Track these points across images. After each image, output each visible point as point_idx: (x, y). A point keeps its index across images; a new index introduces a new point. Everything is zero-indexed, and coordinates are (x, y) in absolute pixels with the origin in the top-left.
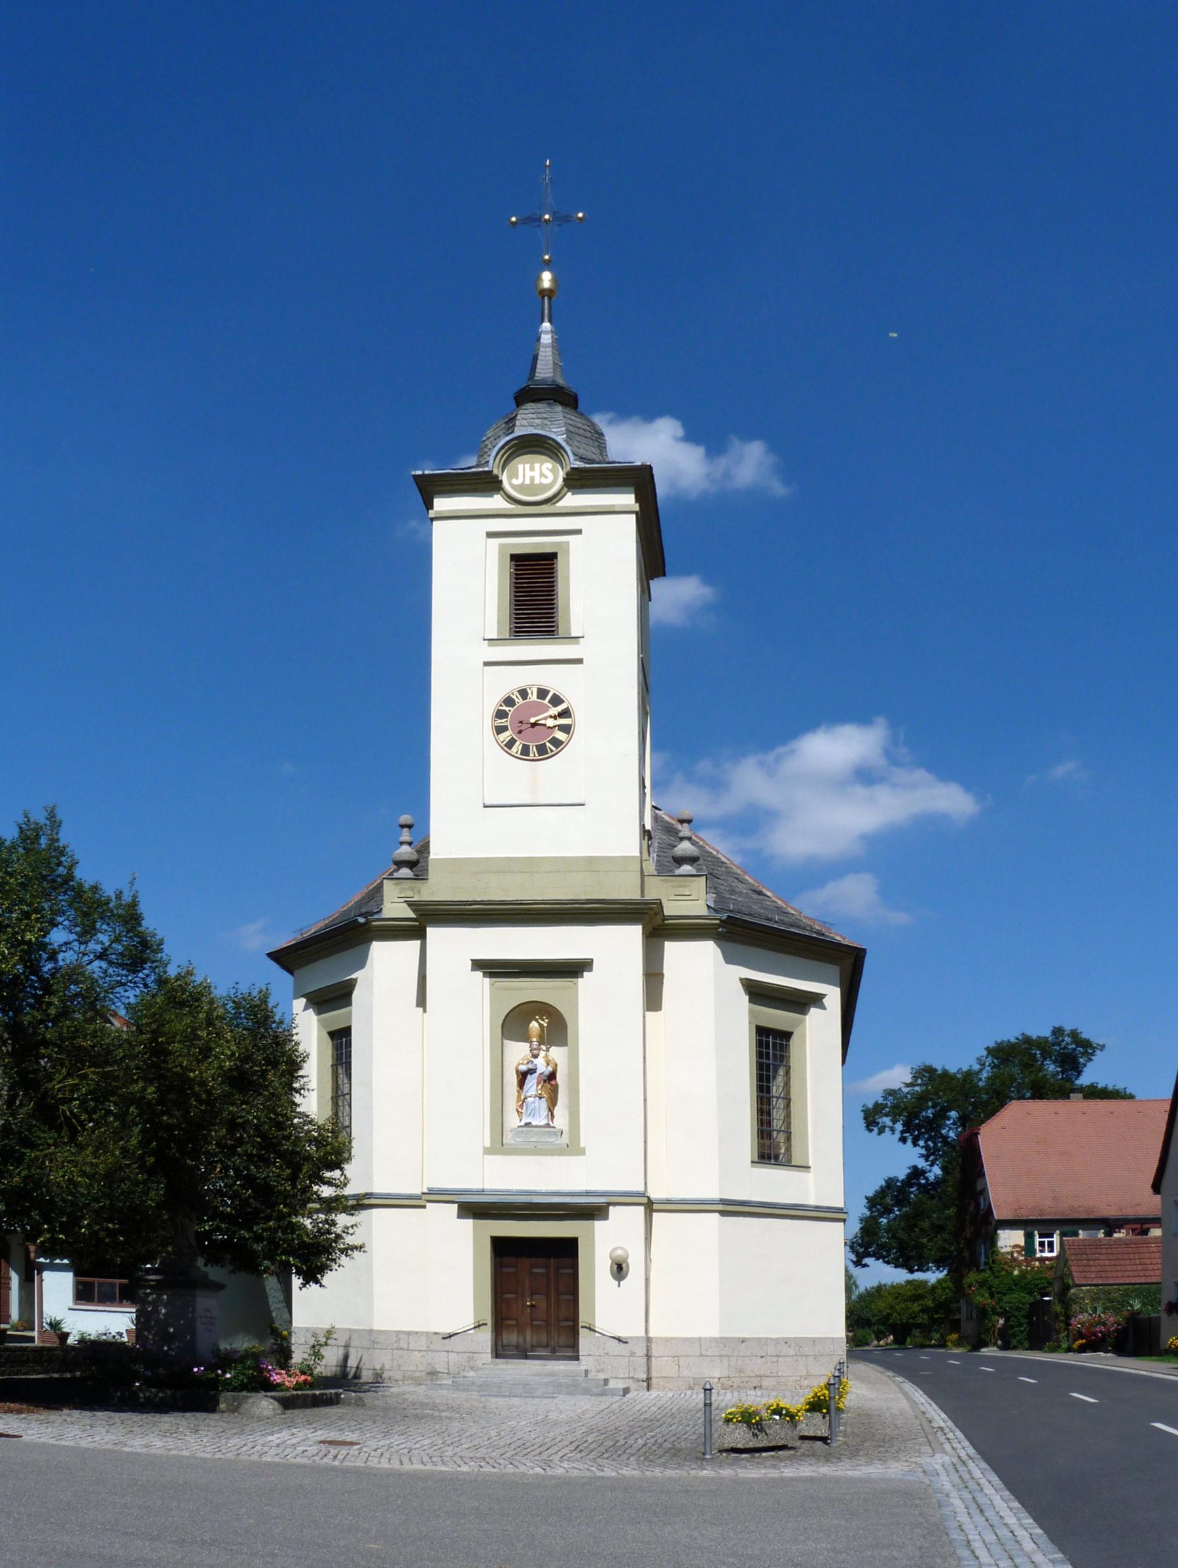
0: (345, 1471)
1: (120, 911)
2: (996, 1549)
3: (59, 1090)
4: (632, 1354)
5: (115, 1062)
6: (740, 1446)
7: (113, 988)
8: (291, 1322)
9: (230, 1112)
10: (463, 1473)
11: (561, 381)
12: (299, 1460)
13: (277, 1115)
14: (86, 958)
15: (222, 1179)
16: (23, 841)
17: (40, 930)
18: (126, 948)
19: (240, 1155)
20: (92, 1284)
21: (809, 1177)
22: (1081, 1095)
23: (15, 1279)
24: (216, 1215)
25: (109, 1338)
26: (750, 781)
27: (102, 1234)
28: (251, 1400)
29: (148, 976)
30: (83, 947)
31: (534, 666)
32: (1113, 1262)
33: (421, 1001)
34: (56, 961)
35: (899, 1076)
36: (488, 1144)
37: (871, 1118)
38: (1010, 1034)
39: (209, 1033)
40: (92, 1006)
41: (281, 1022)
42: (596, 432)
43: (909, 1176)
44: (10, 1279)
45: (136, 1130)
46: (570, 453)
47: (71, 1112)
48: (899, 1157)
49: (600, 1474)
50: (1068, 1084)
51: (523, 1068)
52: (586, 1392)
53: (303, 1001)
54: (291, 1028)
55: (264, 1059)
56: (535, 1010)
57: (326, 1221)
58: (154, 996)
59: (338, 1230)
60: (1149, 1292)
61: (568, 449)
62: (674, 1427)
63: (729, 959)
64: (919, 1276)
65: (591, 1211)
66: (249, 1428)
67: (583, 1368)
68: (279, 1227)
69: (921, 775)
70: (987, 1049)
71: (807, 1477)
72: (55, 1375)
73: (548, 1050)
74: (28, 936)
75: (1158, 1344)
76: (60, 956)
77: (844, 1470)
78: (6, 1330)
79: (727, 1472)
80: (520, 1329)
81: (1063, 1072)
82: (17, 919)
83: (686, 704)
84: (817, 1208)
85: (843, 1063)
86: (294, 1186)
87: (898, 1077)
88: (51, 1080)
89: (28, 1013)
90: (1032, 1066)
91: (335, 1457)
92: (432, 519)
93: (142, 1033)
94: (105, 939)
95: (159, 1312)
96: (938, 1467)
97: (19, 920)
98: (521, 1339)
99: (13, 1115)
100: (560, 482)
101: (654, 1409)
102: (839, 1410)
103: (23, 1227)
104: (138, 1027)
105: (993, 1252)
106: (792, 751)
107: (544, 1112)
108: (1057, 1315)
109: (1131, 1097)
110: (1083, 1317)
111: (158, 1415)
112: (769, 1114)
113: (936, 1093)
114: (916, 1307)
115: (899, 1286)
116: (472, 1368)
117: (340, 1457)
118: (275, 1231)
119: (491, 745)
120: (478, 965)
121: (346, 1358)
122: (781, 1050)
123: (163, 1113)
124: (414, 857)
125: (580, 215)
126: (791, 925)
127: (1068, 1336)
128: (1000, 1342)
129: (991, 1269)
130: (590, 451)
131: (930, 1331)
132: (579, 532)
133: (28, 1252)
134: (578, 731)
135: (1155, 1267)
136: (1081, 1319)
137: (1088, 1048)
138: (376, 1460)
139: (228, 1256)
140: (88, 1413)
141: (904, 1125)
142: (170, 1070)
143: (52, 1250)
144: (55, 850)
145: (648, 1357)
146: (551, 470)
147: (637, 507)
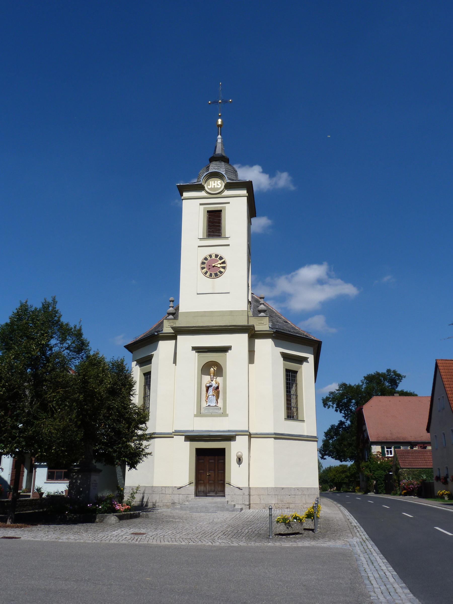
0: (140, 546)
1: (75, 332)
2: (379, 580)
3: (49, 397)
4: (244, 494)
5: (70, 387)
6: (282, 533)
10: (183, 545)
11: (224, 154)
12: (124, 542)
13: (124, 404)
14: (62, 349)
15: (104, 429)
16: (44, 308)
17: (47, 340)
19: (111, 420)
20: (54, 472)
21: (304, 424)
23: (26, 471)
24: (101, 443)
26: (283, 284)
27: (60, 452)
28: (108, 517)
29: (83, 355)
30: (61, 345)
31: (214, 247)
32: (414, 459)
33: (175, 362)
34: (52, 350)
35: (334, 387)
37: (325, 402)
38: (372, 372)
39: (103, 375)
40: (63, 366)
41: (128, 370)
43: (339, 424)
44: (24, 472)
45: (75, 412)
47: (53, 406)
48: (336, 417)
49: (232, 545)
50: (393, 390)
51: (208, 385)
52: (227, 510)
53: (135, 362)
54: (131, 372)
55: (121, 384)
58: (85, 362)
59: (143, 447)
60: (429, 472)
61: (226, 176)
62: (258, 525)
63: (277, 345)
64: (344, 463)
65: (229, 438)
67: (226, 500)
69: (339, 281)
70: (364, 377)
72: (37, 511)
73: (216, 378)
74: (43, 342)
76: (53, 349)
78: (20, 493)
79: (278, 544)
80: (205, 484)
81: (391, 386)
84: (308, 436)
88: (46, 394)
90: (380, 383)
91: (137, 540)
92: (183, 200)
93: (80, 376)
94: (69, 342)
96: (355, 543)
97: (40, 336)
98: (205, 489)
101: (251, 517)
102: (318, 518)
105: (370, 454)
106: (297, 274)
107: (215, 401)
108: (395, 480)
109: (416, 395)
110: (405, 481)
111: (73, 525)
112: (290, 401)
113: (347, 393)
114: (343, 476)
116: (187, 501)
117: (139, 540)
119: (200, 273)
120: (194, 348)
121: (143, 498)
122: (294, 378)
127: (400, 489)
129: (370, 461)
130: (233, 177)
132: (229, 203)
133: (32, 461)
134: (228, 268)
138: (151, 541)
139: (104, 459)
140: (47, 526)
141: (337, 405)
142: (88, 389)
145: (249, 495)
147: (247, 195)
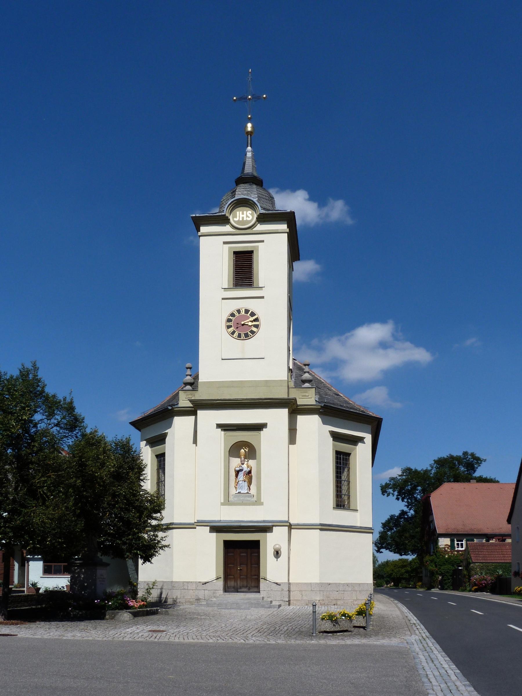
1: (65, 406)
2: (439, 678)
3: (38, 483)
4: (282, 590)
5: (63, 470)
6: (328, 630)
11: (255, 174)
12: (140, 639)
14: (50, 426)
15: (109, 518)
16: (22, 376)
17: (30, 414)
18: (68, 421)
21: (358, 514)
24: (107, 534)
25: (59, 589)
26: (335, 348)
27: (56, 544)
29: (77, 433)
30: (49, 421)
31: (243, 300)
33: (195, 441)
34: (37, 427)
36: (222, 501)
37: (384, 489)
38: (444, 454)
39: (104, 457)
40: (53, 446)
41: (135, 451)
42: (271, 197)
43: (400, 514)
45: (72, 499)
46: (259, 206)
47: (43, 492)
48: (396, 506)
49: (268, 642)
50: (469, 476)
51: (238, 469)
52: (263, 606)
53: (145, 442)
54: (139, 454)
55: (128, 467)
56: (243, 445)
57: (154, 535)
59: (159, 539)
60: (506, 566)
61: (258, 204)
62: (300, 622)
63: (324, 423)
64: (404, 557)
67: (262, 596)
68: (134, 538)
69: (408, 344)
70: (434, 460)
72: (34, 607)
73: (248, 461)
74: (24, 417)
75: (510, 589)
76: (39, 426)
77: (373, 641)
78: (12, 588)
79: (322, 642)
80: (235, 579)
82: (19, 410)
83: (308, 315)
85: (372, 466)
86: (140, 521)
87: (396, 472)
88: (34, 479)
89: (24, 450)
90: (454, 468)
91: (156, 637)
92: (200, 236)
93: (75, 457)
94: (58, 417)
95: (80, 577)
96: (413, 641)
99: (17, 495)
100: (255, 219)
102: (370, 615)
103: (21, 542)
104: (73, 455)
105: (437, 548)
106: (353, 335)
107: (247, 487)
108: (465, 576)
109: (498, 482)
110: (477, 577)
111: (79, 622)
112: (341, 488)
114: (403, 571)
115: (396, 561)
116: (214, 597)
117: (158, 637)
118: (132, 540)
119: (225, 334)
120: (219, 426)
121: (161, 594)
122: (346, 461)
123: (84, 491)
124: (192, 381)
125: (264, 96)
126: (351, 408)
127: (470, 585)
128: (440, 587)
129: (435, 554)
130: (268, 206)
131: (409, 581)
132: (263, 241)
133: (23, 553)
134: (262, 327)
135: (509, 556)
136: (475, 577)
137: (478, 460)
138: (173, 638)
139: (111, 551)
140: (48, 623)
141: (398, 493)
142: (87, 473)
143: (34, 552)
144: (36, 380)
145: (289, 591)
147: (288, 230)
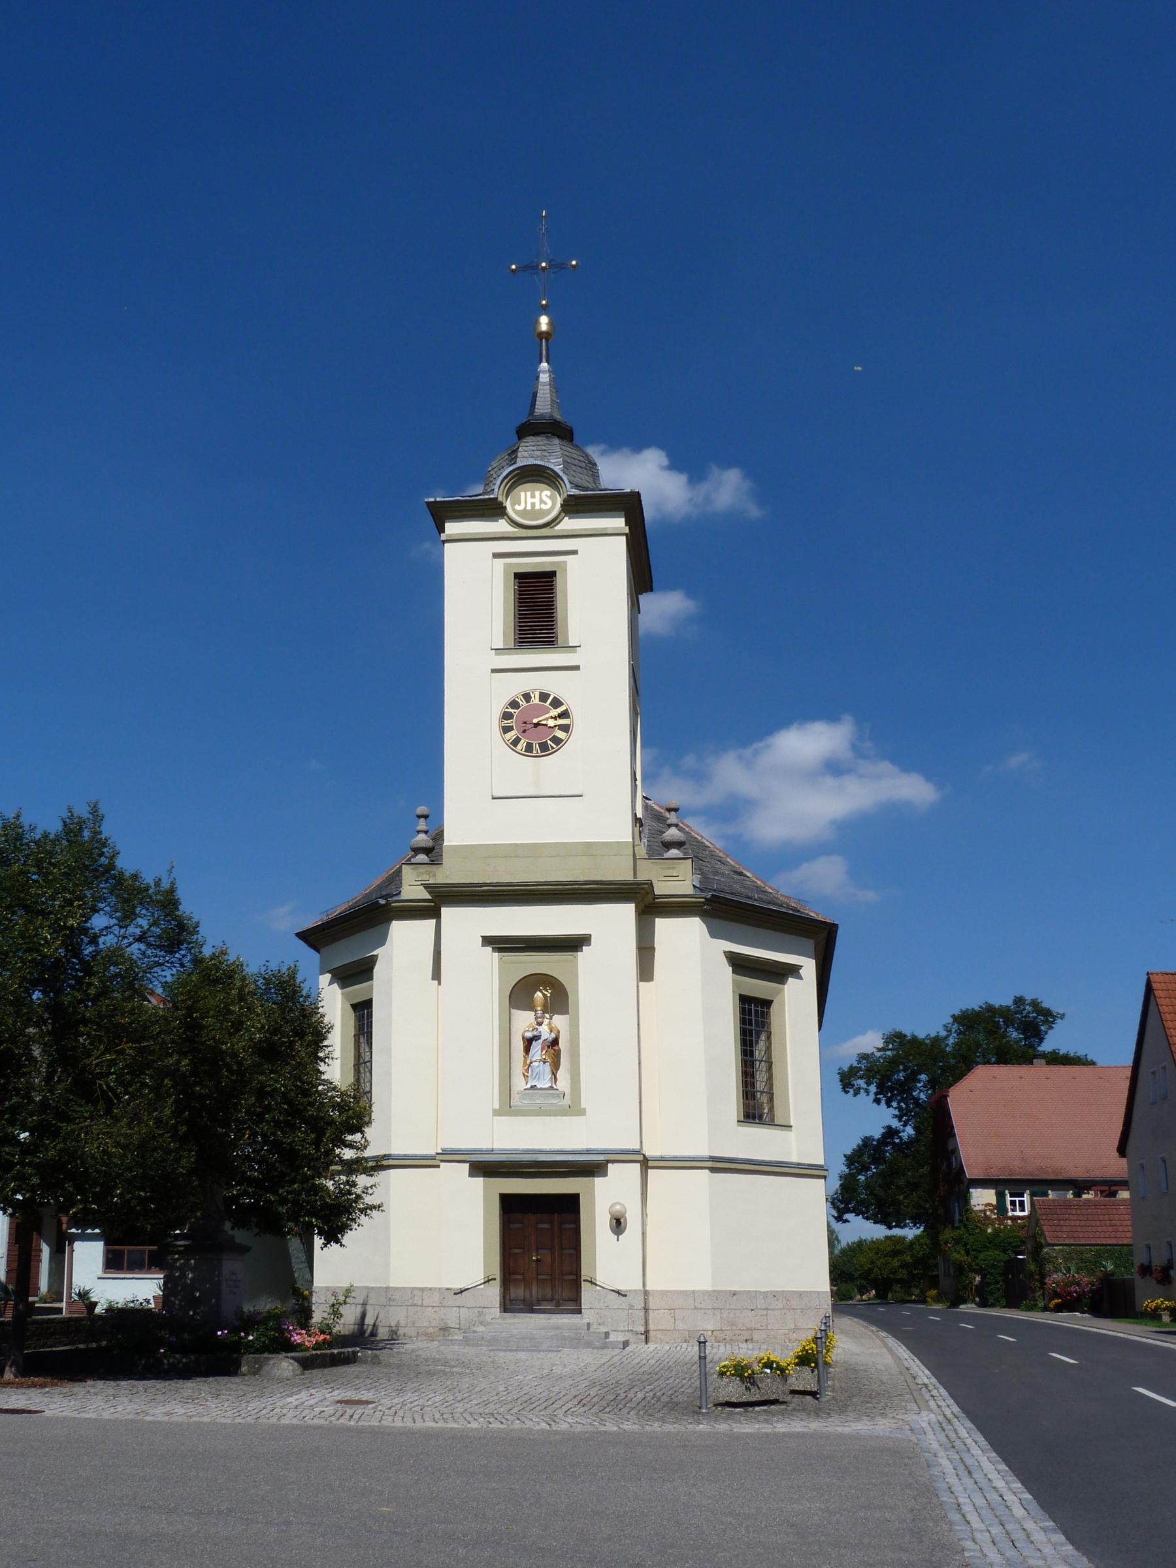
0: (359, 1431)
3: (97, 1065)
4: (631, 1307)
5: (152, 1037)
6: (734, 1400)
7: (151, 968)
8: (312, 1281)
9: (259, 1082)
11: (558, 416)
12: (316, 1421)
13: (303, 1082)
14: (126, 941)
15: (250, 1145)
16: (67, 834)
17: (82, 916)
18: (164, 931)
20: (122, 1252)
21: (791, 1135)
22: (1043, 1061)
23: (46, 1251)
26: (730, 774)
27: (134, 1202)
29: (184, 956)
30: (123, 931)
32: (1083, 1223)
33: (437, 975)
34: (97, 944)
36: (497, 1106)
37: (847, 1080)
38: (974, 1002)
39: (241, 1008)
40: (131, 985)
41: (308, 996)
43: (884, 1135)
44: (41, 1251)
45: (170, 1101)
47: (108, 1086)
48: (874, 1118)
50: (1030, 1050)
51: (529, 1035)
52: (589, 1345)
53: (328, 976)
54: (317, 1001)
55: (292, 1031)
56: (539, 983)
57: (347, 1182)
58: (189, 975)
59: (358, 1191)
60: (1121, 1253)
61: (565, 478)
62: (671, 1380)
63: (714, 934)
64: (897, 1232)
65: (591, 1168)
66: (269, 1390)
67: (586, 1321)
69: (885, 766)
70: (953, 1016)
71: (798, 1433)
72: (81, 1346)
73: (551, 1018)
74: (71, 922)
76: (101, 940)
78: (34, 1303)
79: (722, 1427)
80: (527, 1284)
81: (1025, 1039)
82: (60, 906)
83: (673, 705)
84: (800, 1166)
87: (871, 1042)
88: (89, 1056)
90: (996, 1033)
91: (351, 1417)
92: (444, 542)
94: (144, 923)
95: (186, 1277)
96: (924, 1425)
99: (51, 1091)
101: (652, 1362)
102: (826, 1364)
103: (56, 1199)
104: (174, 1003)
105: (967, 1210)
106: (768, 746)
107: (549, 1076)
108: (1032, 1274)
109: (1093, 1063)
110: (1058, 1276)
111: (181, 1381)
112: (753, 1076)
114: (895, 1263)
116: (481, 1323)
117: (356, 1417)
119: (499, 744)
120: (488, 941)
121: (363, 1315)
122: (763, 1017)
123: (196, 1084)
125: (574, 263)
126: (769, 903)
127: (1043, 1295)
129: (965, 1226)
130: (585, 480)
131: (910, 1287)
132: (575, 552)
133: (60, 1223)
134: (575, 730)
136: (1055, 1278)
137: (1049, 1016)
138: (390, 1419)
139: (254, 1220)
140: (112, 1383)
141: (877, 1087)
142: (203, 1043)
143: (84, 1221)
145: (646, 1309)
146: (550, 497)
147: (627, 530)
